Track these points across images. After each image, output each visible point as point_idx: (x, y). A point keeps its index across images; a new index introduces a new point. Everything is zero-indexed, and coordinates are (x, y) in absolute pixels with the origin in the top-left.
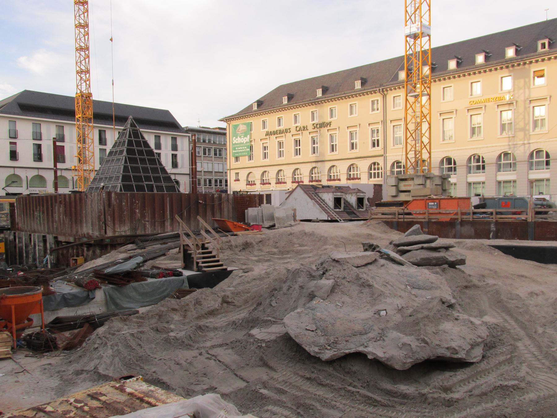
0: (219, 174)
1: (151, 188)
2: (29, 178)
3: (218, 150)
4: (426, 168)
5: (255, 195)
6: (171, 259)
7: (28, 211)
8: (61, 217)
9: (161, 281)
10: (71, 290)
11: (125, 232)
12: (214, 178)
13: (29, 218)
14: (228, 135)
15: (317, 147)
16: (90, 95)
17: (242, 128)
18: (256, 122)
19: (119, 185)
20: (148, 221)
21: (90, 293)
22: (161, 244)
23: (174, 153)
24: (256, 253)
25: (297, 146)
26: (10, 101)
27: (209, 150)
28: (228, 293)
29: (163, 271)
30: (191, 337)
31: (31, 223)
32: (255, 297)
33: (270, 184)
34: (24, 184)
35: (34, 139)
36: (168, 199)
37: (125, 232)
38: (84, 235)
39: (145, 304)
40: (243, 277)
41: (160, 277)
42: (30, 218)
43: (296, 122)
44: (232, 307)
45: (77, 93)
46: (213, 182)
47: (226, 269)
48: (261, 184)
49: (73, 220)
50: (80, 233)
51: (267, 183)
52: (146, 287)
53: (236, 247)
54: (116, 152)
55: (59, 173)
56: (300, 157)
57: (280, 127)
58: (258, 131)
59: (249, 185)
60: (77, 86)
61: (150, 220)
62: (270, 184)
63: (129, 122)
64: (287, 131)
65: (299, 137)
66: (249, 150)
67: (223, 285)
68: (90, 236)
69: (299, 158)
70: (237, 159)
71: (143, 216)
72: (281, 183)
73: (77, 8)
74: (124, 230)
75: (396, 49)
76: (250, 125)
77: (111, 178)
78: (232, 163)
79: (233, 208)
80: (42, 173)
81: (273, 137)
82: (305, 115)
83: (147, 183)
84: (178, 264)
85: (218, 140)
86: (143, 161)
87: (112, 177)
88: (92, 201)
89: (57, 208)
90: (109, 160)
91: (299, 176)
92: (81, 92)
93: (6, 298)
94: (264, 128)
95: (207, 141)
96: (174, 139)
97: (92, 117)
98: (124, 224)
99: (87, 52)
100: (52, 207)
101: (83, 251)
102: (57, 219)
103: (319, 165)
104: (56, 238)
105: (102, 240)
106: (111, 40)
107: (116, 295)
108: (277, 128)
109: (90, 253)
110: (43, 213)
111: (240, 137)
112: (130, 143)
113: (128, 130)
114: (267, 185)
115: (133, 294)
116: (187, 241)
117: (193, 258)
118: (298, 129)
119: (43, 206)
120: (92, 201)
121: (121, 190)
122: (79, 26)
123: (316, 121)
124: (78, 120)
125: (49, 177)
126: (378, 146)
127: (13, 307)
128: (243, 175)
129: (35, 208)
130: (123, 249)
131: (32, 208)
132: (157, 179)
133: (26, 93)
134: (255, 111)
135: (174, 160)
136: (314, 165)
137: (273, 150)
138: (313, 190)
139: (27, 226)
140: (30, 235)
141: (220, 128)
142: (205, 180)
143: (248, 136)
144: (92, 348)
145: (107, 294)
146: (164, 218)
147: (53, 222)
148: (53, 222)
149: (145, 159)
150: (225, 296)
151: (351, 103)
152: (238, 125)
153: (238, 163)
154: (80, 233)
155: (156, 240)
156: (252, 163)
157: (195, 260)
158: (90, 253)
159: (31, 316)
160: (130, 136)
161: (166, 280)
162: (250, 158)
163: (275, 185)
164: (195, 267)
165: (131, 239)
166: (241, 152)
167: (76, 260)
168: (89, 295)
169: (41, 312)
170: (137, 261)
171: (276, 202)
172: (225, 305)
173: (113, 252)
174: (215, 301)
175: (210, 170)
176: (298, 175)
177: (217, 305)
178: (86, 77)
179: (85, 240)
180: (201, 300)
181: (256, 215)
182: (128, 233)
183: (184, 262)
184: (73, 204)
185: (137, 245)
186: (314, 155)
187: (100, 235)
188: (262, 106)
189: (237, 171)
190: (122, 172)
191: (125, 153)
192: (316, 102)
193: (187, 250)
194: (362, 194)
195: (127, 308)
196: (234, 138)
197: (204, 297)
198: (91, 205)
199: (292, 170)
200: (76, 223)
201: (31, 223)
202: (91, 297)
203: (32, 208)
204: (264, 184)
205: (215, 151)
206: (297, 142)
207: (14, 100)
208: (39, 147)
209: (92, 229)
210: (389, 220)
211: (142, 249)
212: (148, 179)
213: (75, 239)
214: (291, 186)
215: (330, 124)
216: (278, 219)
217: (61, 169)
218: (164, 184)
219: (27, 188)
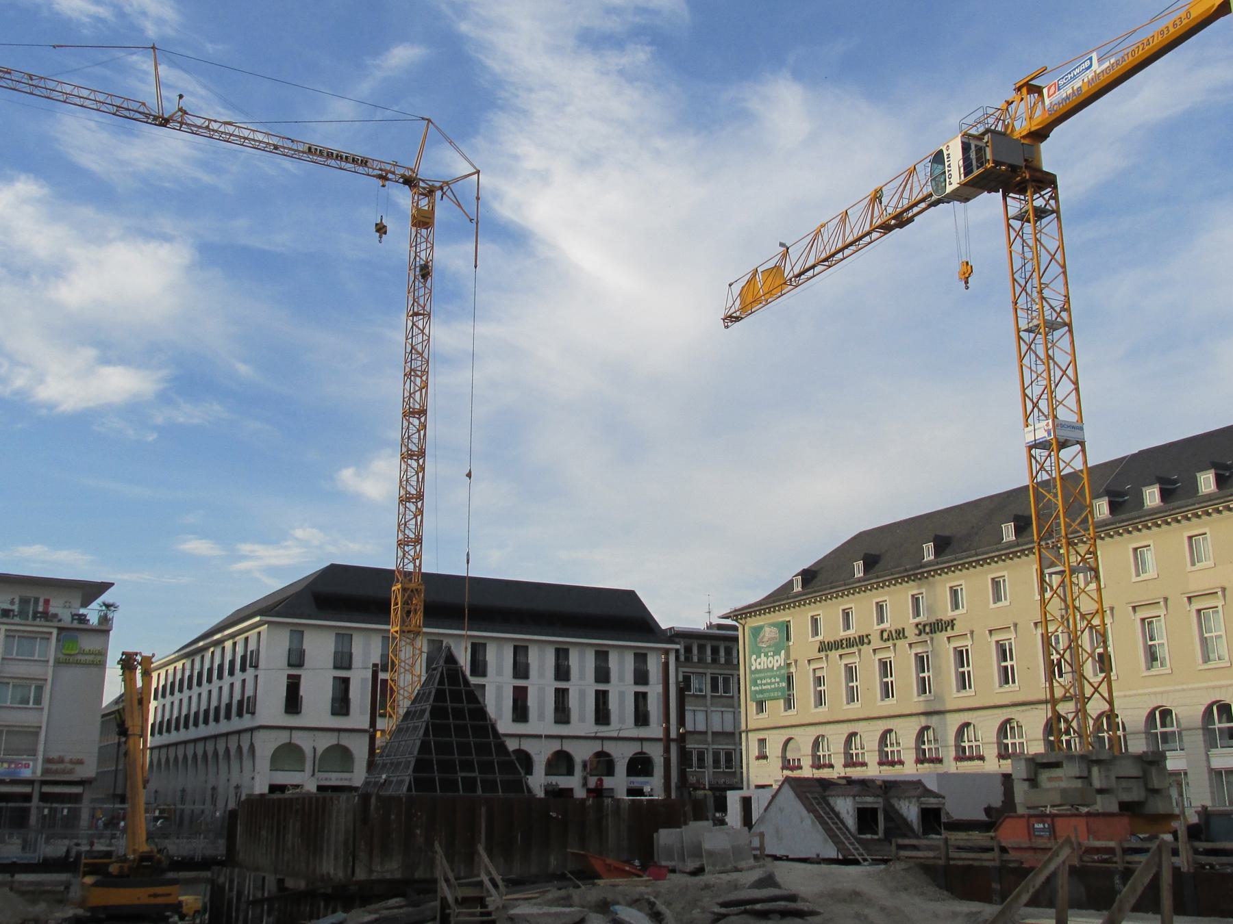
1: (470, 785)
2: (320, 751)
4: (1217, 725)
15: (1012, 667)
17: (769, 633)
18: (799, 619)
19: (407, 779)
23: (641, 689)
34: (308, 765)
36: (483, 809)
43: (881, 620)
46: (709, 759)
56: (1015, 687)
57: (848, 632)
58: (803, 643)
64: (862, 640)
66: (784, 684)
70: (761, 706)
74: (391, 869)
75: (1006, 471)
78: (751, 717)
80: (346, 741)
81: (834, 654)
82: (897, 602)
83: (463, 774)
86: (461, 731)
91: (895, 748)
94: (817, 634)
96: (641, 658)
102: (289, 844)
103: (934, 721)
104: (281, 882)
106: (469, 475)
108: (843, 634)
111: (766, 655)
118: (885, 635)
121: (409, 789)
123: (922, 619)
126: (1014, 682)
132: (486, 767)
133: (335, 572)
135: (641, 708)
136: (923, 721)
137: (836, 686)
138: (819, 789)
142: (716, 755)
151: (952, 584)
152: (760, 628)
153: (764, 715)
156: (792, 716)
160: (441, 682)
162: (789, 705)
176: (892, 745)
182: (398, 875)
186: (922, 698)
189: (761, 735)
190: (416, 753)
191: (427, 715)
192: (916, 572)
194: (933, 800)
199: (997, 725)
206: (885, 667)
207: (307, 586)
208: (346, 681)
210: (931, 862)
212: (467, 766)
215: (951, 623)
216: (711, 854)
219: (313, 775)
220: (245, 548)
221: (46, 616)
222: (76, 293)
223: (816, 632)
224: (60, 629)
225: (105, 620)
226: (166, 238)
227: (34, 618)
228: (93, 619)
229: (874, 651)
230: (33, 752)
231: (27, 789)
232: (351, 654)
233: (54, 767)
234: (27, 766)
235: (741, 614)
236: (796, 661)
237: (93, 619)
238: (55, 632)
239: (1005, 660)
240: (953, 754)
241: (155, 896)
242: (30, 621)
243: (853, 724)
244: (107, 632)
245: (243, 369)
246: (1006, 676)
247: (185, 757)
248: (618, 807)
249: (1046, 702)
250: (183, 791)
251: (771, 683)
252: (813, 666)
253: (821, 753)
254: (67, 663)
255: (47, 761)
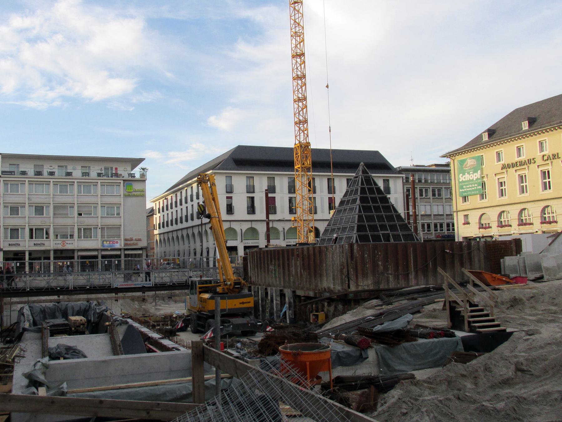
0: (439, 217)
1: (387, 237)
3: (436, 190)
5: (510, 242)
6: (428, 317)
7: (262, 265)
8: (299, 270)
9: (433, 342)
10: (343, 348)
11: (368, 286)
12: (434, 222)
13: (263, 272)
14: (452, 172)
15: (505, 189)
16: (308, 144)
18: (488, 154)
20: (391, 274)
21: (363, 352)
22: (408, 300)
24: (528, 311)
25: (545, 178)
26: (226, 157)
27: (426, 191)
28: (522, 359)
29: (430, 331)
30: (515, 410)
31: (265, 277)
32: (555, 366)
33: (511, 226)
35: (247, 192)
36: (412, 249)
37: (368, 286)
38: (325, 289)
39: (417, 367)
40: (530, 341)
41: (431, 337)
42: (264, 271)
43: (542, 150)
44: (528, 376)
45: (295, 144)
46: (432, 227)
47: (505, 330)
48: (498, 226)
49: (313, 274)
50: (320, 286)
51: (506, 226)
52: (418, 348)
53: (503, 303)
54: (348, 201)
55: (271, 226)
57: (520, 158)
59: (482, 228)
60: (296, 137)
61: (393, 273)
62: (511, 226)
63: (361, 168)
65: (549, 168)
66: (480, 187)
67: (504, 349)
68: (332, 290)
69: (548, 193)
70: (465, 199)
71: (386, 269)
72: (525, 224)
73: (294, 62)
74: (367, 284)
76: (481, 160)
77: (344, 229)
78: (458, 203)
79: (484, 256)
80: (255, 225)
83: (382, 232)
84: (443, 322)
85: (435, 178)
86: (377, 209)
87: (346, 228)
88: (333, 254)
89: (293, 261)
90: (341, 210)
92: (300, 142)
93: (302, 354)
95: (423, 181)
97: (311, 166)
98: (367, 277)
99: (304, 103)
100: (288, 259)
101: (323, 306)
102: (294, 272)
104: (294, 292)
105: (346, 295)
106: (327, 87)
107: (388, 355)
108: (517, 159)
109: (332, 309)
110: (279, 266)
111: (469, 173)
112: (363, 191)
113: (360, 177)
114: (506, 228)
115: (405, 355)
116: (454, 296)
117: (463, 317)
118: (545, 158)
119: (279, 259)
120: (333, 254)
122: (298, 78)
124: (297, 171)
125: (262, 229)
126: (527, 192)
127: (308, 363)
128: (474, 217)
129: (269, 262)
130: (367, 304)
131: (266, 262)
132: (393, 228)
133: (240, 149)
134: (486, 142)
139: (261, 280)
140: (266, 289)
141: (436, 165)
143: (479, 171)
144: (399, 413)
145: (379, 354)
146: (408, 271)
147: (289, 276)
148: (289, 276)
149: (379, 206)
150: (518, 362)
152: (465, 160)
153: (467, 203)
154: (320, 286)
155: (402, 295)
157: (466, 319)
158: (332, 309)
159: (320, 374)
160: (362, 184)
161: (438, 341)
162: (483, 196)
163: (517, 227)
164: (466, 327)
165: (374, 294)
166: (470, 191)
167: (317, 316)
168: (361, 354)
169: (330, 370)
170: (408, 319)
171: (527, 247)
172: (519, 373)
173: (360, 309)
174: (508, 368)
175: (428, 213)
176: (549, 213)
177: (511, 373)
178: (304, 127)
179: (327, 295)
180: (492, 366)
181: (514, 266)
182: (371, 288)
183: (451, 320)
184: (312, 257)
185: (382, 300)
187: (343, 289)
188: (494, 135)
189: (466, 213)
190: (356, 222)
191: (358, 202)
193: (455, 307)
195: (399, 371)
196: (461, 175)
197: (493, 362)
198: (332, 258)
199: (541, 209)
200: (315, 276)
201: (265, 277)
202: (364, 356)
203: (266, 262)
204: (502, 226)
205: (433, 191)
206: (545, 174)
208: (252, 199)
209: (334, 283)
211: (388, 304)
212: (383, 227)
213: (315, 294)
214: (540, 228)
216: (547, 269)
217: (273, 221)
218: (400, 233)
220: (172, 154)
221: (117, 175)
222: (96, 47)
223: (499, 159)
224: (124, 180)
225: (143, 175)
226: (133, 17)
227: (112, 176)
228: (138, 176)
229: (538, 166)
230: (119, 236)
231: (119, 253)
232: (254, 186)
233: (129, 242)
234: (117, 243)
235: (451, 155)
236: (487, 175)
237: (138, 176)
238: (122, 182)
239: (523, 183)
240: (496, 224)
241: (243, 303)
242: (110, 178)
243: (524, 204)
244: (145, 181)
245: (169, 75)
246: (502, 193)
247: (168, 238)
248: (479, 246)
249: (459, 211)
250: (179, 251)
251: (472, 187)
252: (498, 177)
253: (502, 220)
254: (129, 196)
255: (126, 240)
